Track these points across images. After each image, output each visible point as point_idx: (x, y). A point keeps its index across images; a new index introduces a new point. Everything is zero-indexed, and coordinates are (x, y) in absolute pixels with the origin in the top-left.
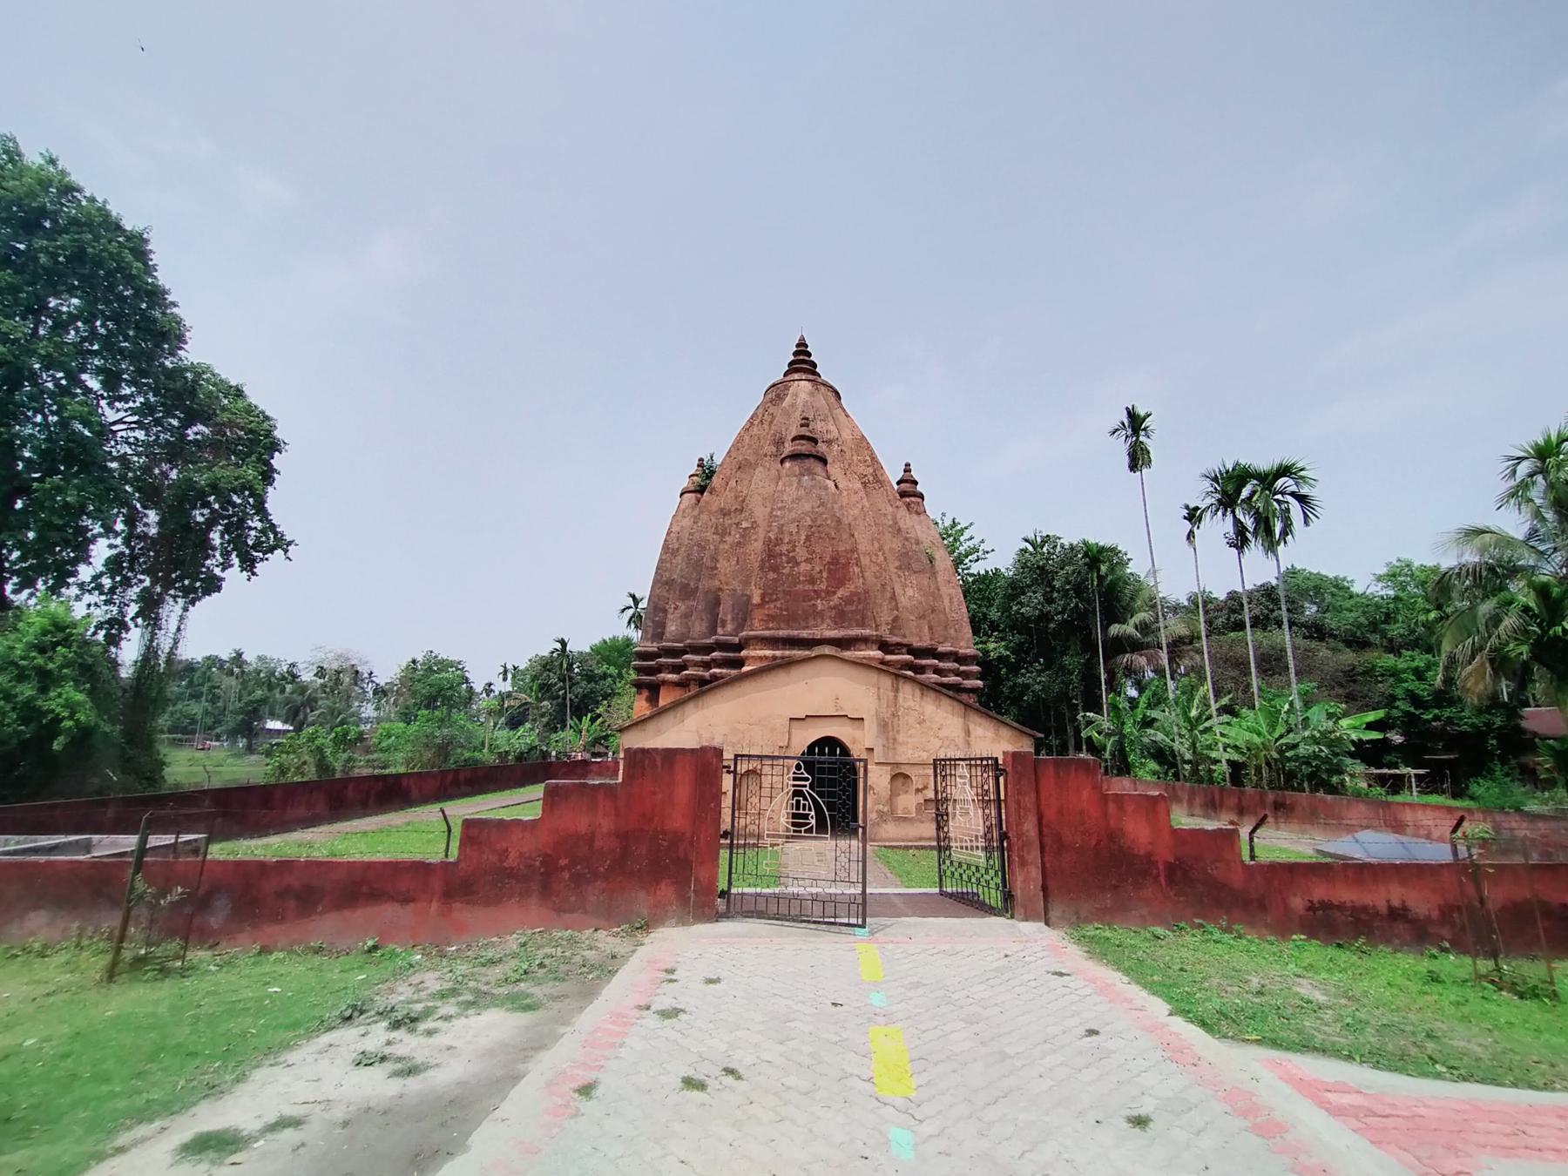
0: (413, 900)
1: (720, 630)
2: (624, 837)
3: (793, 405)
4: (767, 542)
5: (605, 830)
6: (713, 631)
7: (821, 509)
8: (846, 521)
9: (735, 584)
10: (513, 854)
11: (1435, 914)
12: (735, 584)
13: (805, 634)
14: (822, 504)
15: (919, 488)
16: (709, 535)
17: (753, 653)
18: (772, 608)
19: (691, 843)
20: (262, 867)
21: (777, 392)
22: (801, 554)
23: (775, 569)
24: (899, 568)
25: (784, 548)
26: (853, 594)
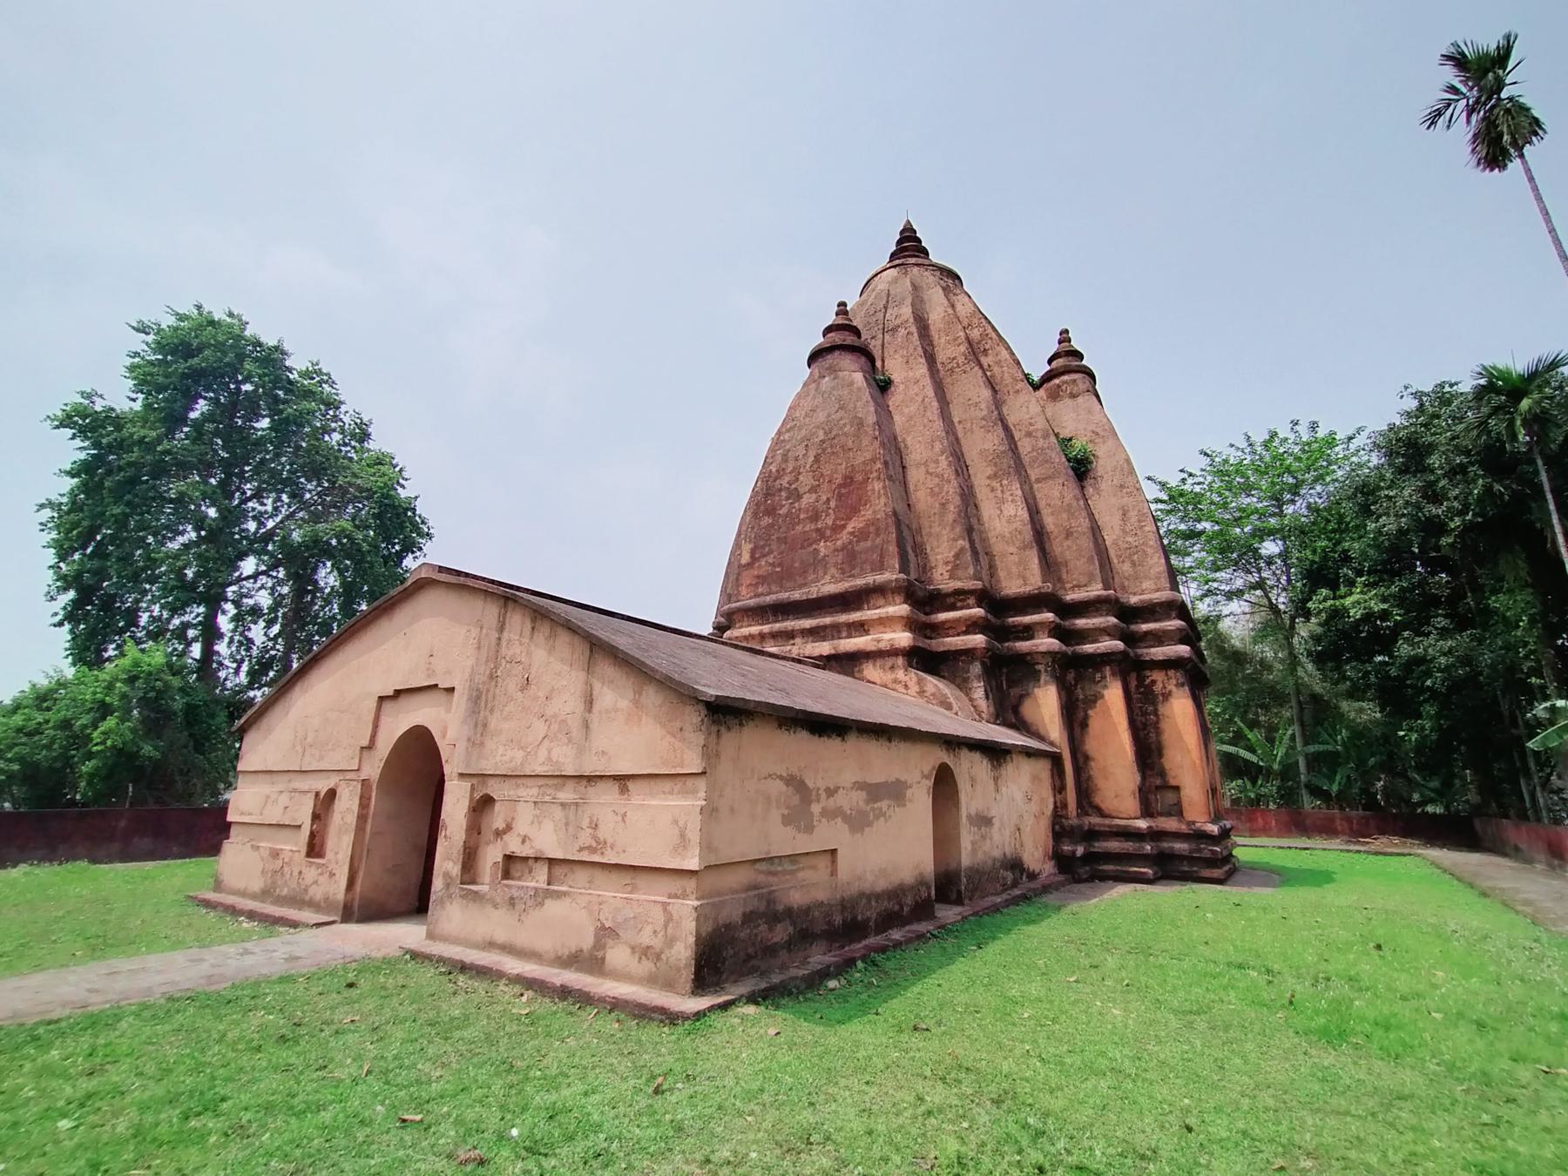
7: (841, 413)
13: (797, 595)
18: (763, 566)
23: (771, 512)
24: (994, 476)
25: (784, 482)
26: (872, 522)
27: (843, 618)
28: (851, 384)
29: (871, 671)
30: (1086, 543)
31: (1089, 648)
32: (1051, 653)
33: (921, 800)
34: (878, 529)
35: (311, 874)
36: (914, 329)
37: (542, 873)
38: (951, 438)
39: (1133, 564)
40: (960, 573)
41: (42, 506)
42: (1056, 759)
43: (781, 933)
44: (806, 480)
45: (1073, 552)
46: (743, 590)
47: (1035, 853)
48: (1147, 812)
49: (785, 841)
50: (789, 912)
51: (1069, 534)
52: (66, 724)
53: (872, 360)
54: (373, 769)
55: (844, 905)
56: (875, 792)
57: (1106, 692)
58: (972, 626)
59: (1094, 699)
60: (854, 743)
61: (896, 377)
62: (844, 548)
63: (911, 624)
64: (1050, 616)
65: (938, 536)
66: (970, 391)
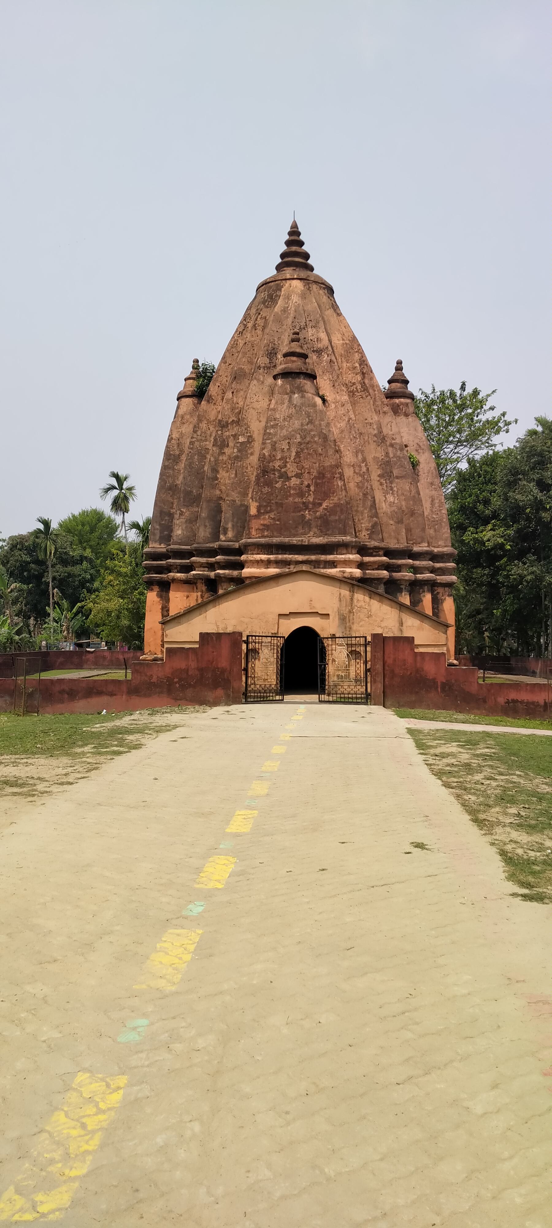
0: (115, 695)
1: (222, 537)
2: (201, 670)
3: (285, 310)
4: (262, 458)
5: (193, 667)
6: (216, 538)
7: (310, 427)
8: (347, 382)
9: (235, 496)
10: (155, 677)
12: (235, 496)
13: (295, 540)
14: (311, 422)
16: (209, 445)
17: (251, 557)
18: (266, 520)
19: (230, 673)
20: (52, 681)
21: (269, 291)
22: (291, 469)
23: (269, 484)
25: (277, 464)
26: (336, 505)
27: (323, 557)
34: (342, 510)
39: (435, 531)
40: (374, 536)
57: (424, 599)
62: (321, 517)
65: (362, 513)
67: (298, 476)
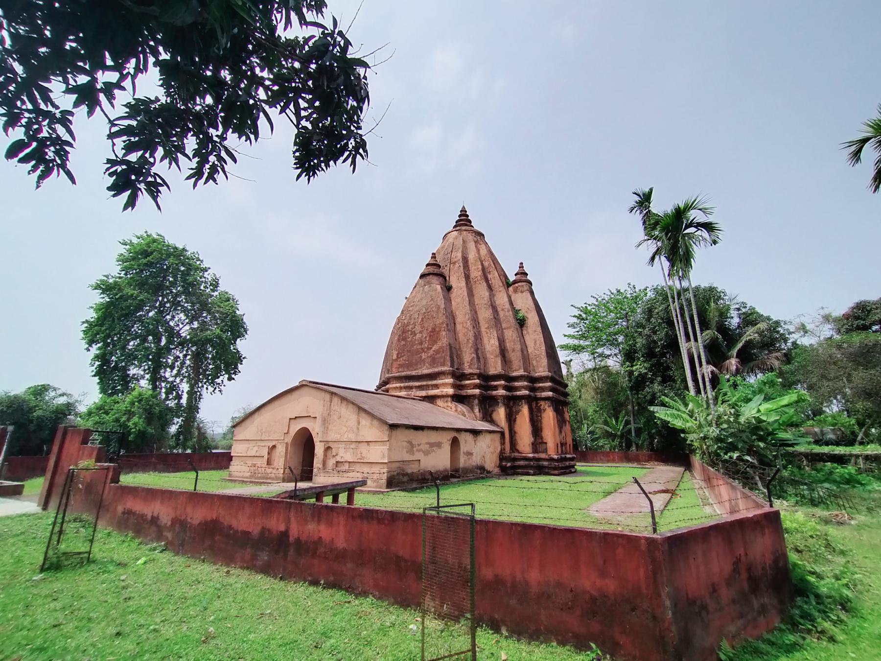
11: (169, 523)
13: (414, 373)
15: (528, 277)
18: (401, 361)
22: (418, 328)
23: (404, 339)
24: (488, 328)
25: (410, 327)
26: (441, 347)
27: (430, 383)
28: (436, 290)
29: (439, 402)
30: (519, 354)
31: (518, 393)
32: (504, 397)
33: (447, 448)
35: (269, 471)
36: (461, 265)
37: (347, 465)
38: (473, 312)
41: (83, 323)
42: (502, 434)
43: (405, 479)
44: (418, 328)
45: (515, 357)
46: (394, 370)
47: (491, 463)
48: (535, 450)
49: (407, 457)
50: (407, 474)
51: (514, 350)
52: (117, 420)
53: (445, 278)
54: (289, 439)
55: (422, 474)
56: (432, 445)
58: (476, 386)
59: (518, 412)
60: (426, 432)
61: (454, 286)
63: (454, 386)
64: (503, 382)
66: (481, 291)
67: (421, 332)
